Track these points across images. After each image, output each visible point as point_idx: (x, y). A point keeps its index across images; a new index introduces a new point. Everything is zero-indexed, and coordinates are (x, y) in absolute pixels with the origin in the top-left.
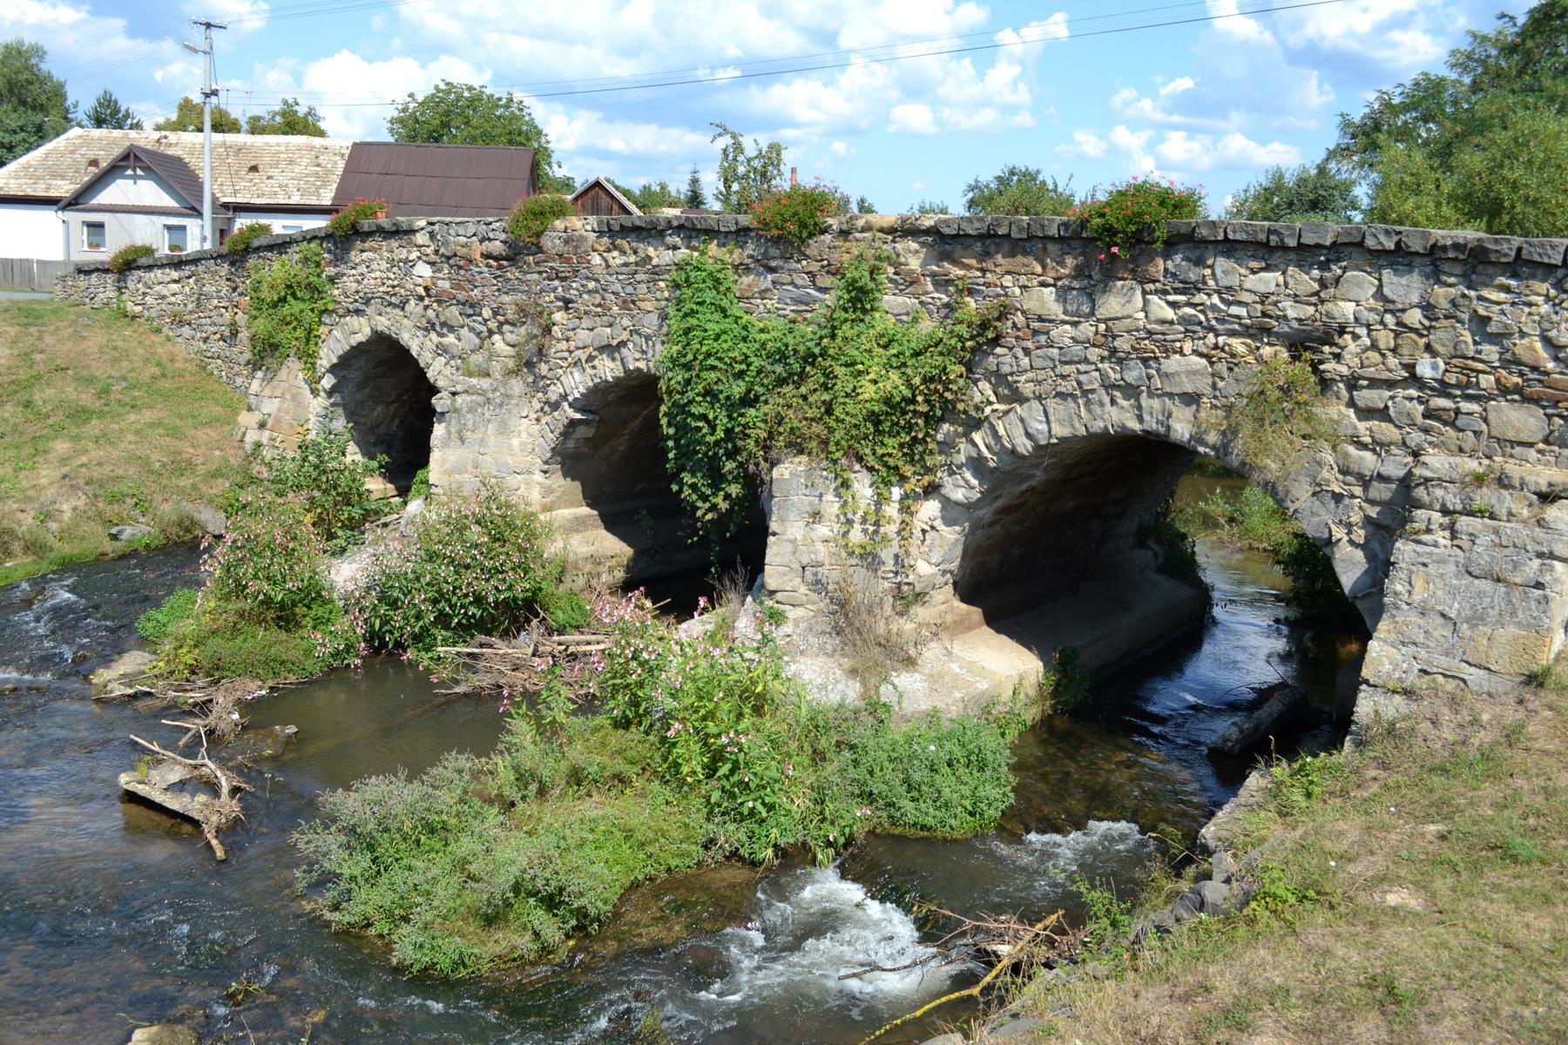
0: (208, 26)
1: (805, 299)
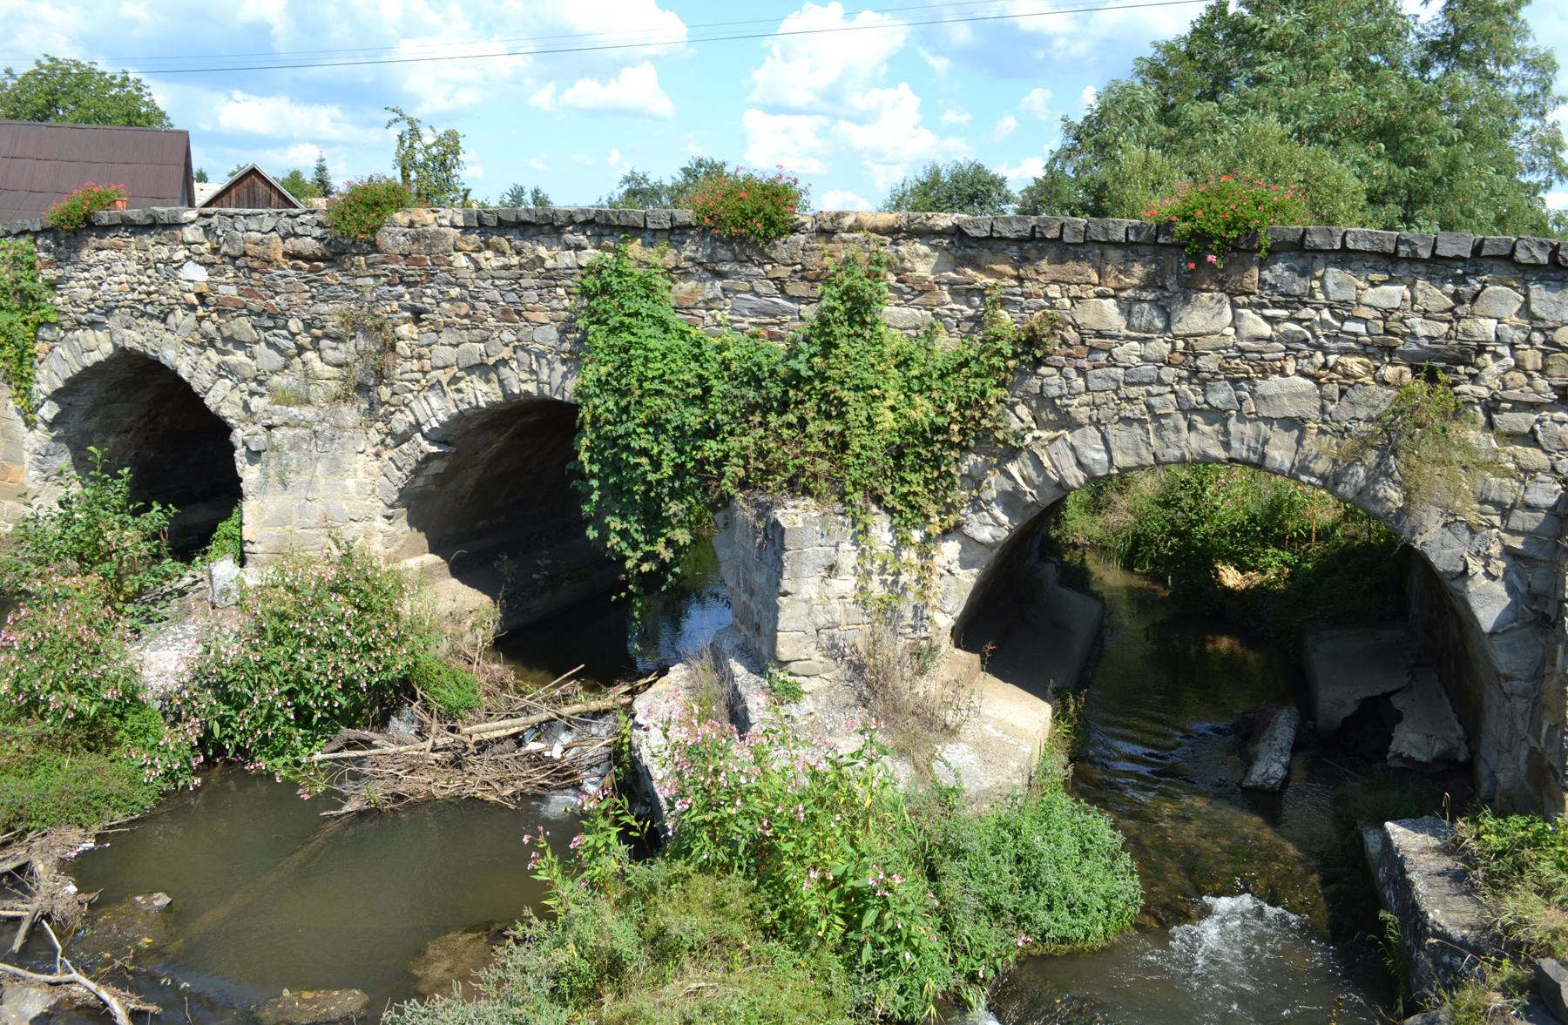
1: (770, 309)
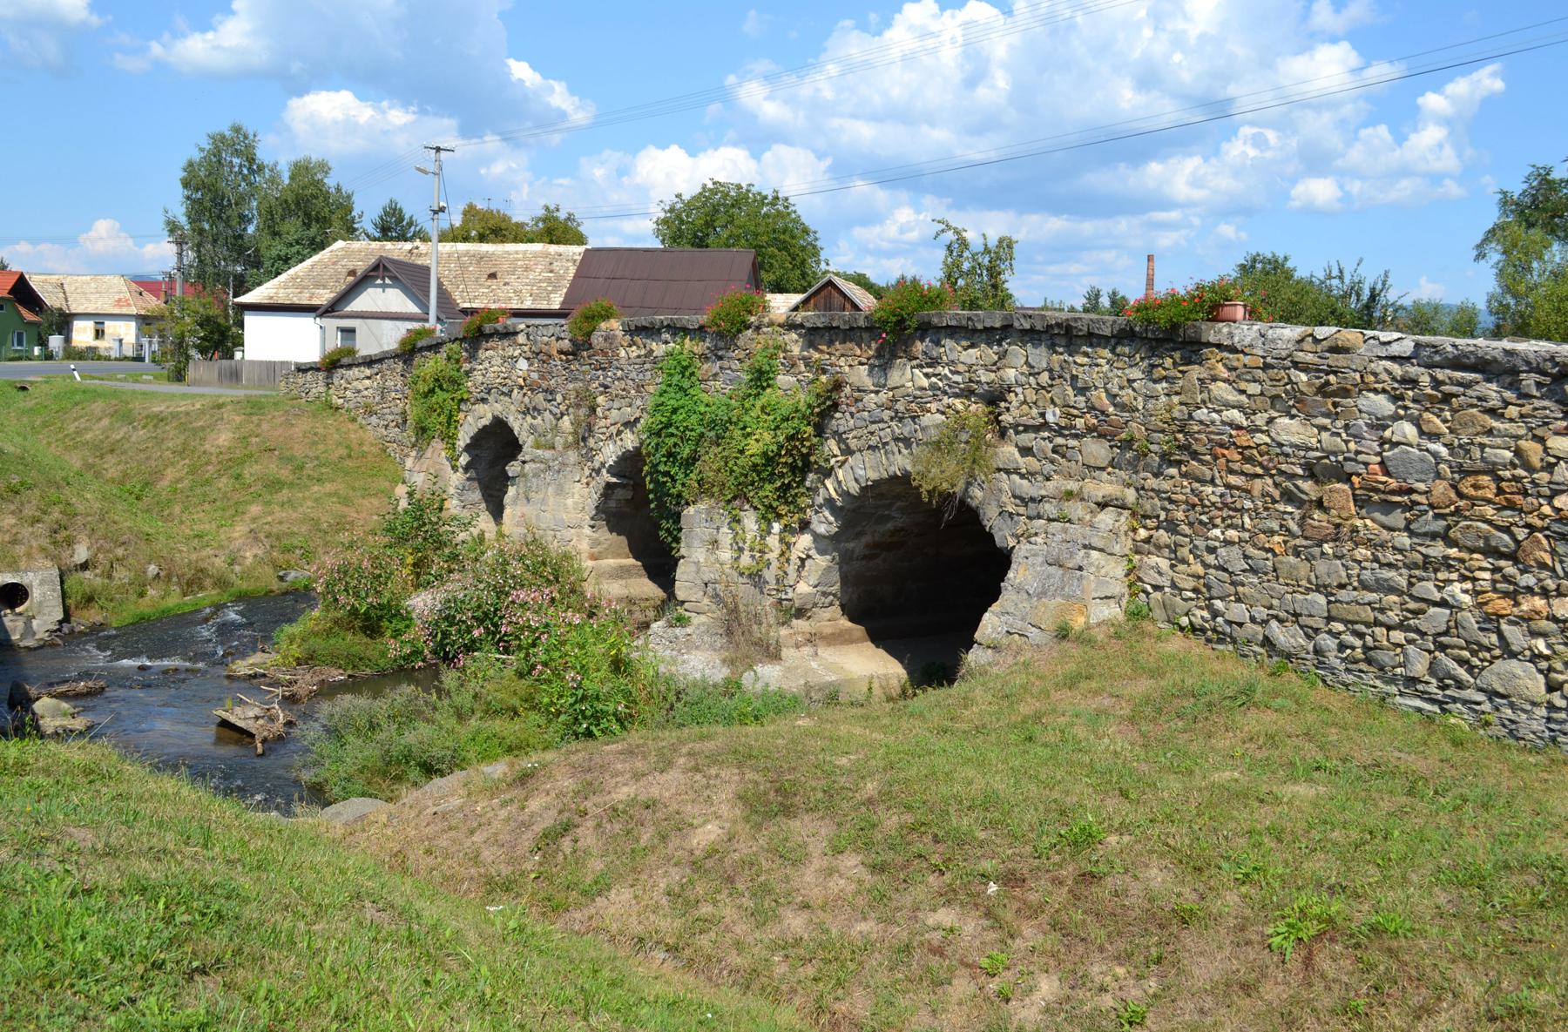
0: (438, 149)
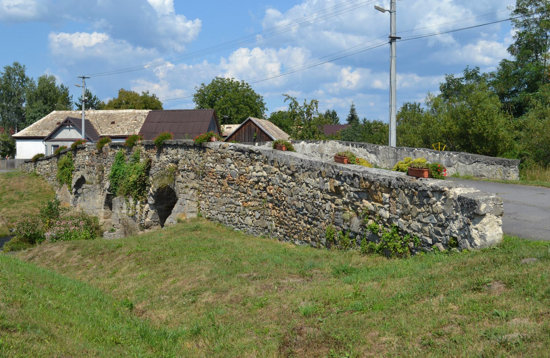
0: (84, 78)
